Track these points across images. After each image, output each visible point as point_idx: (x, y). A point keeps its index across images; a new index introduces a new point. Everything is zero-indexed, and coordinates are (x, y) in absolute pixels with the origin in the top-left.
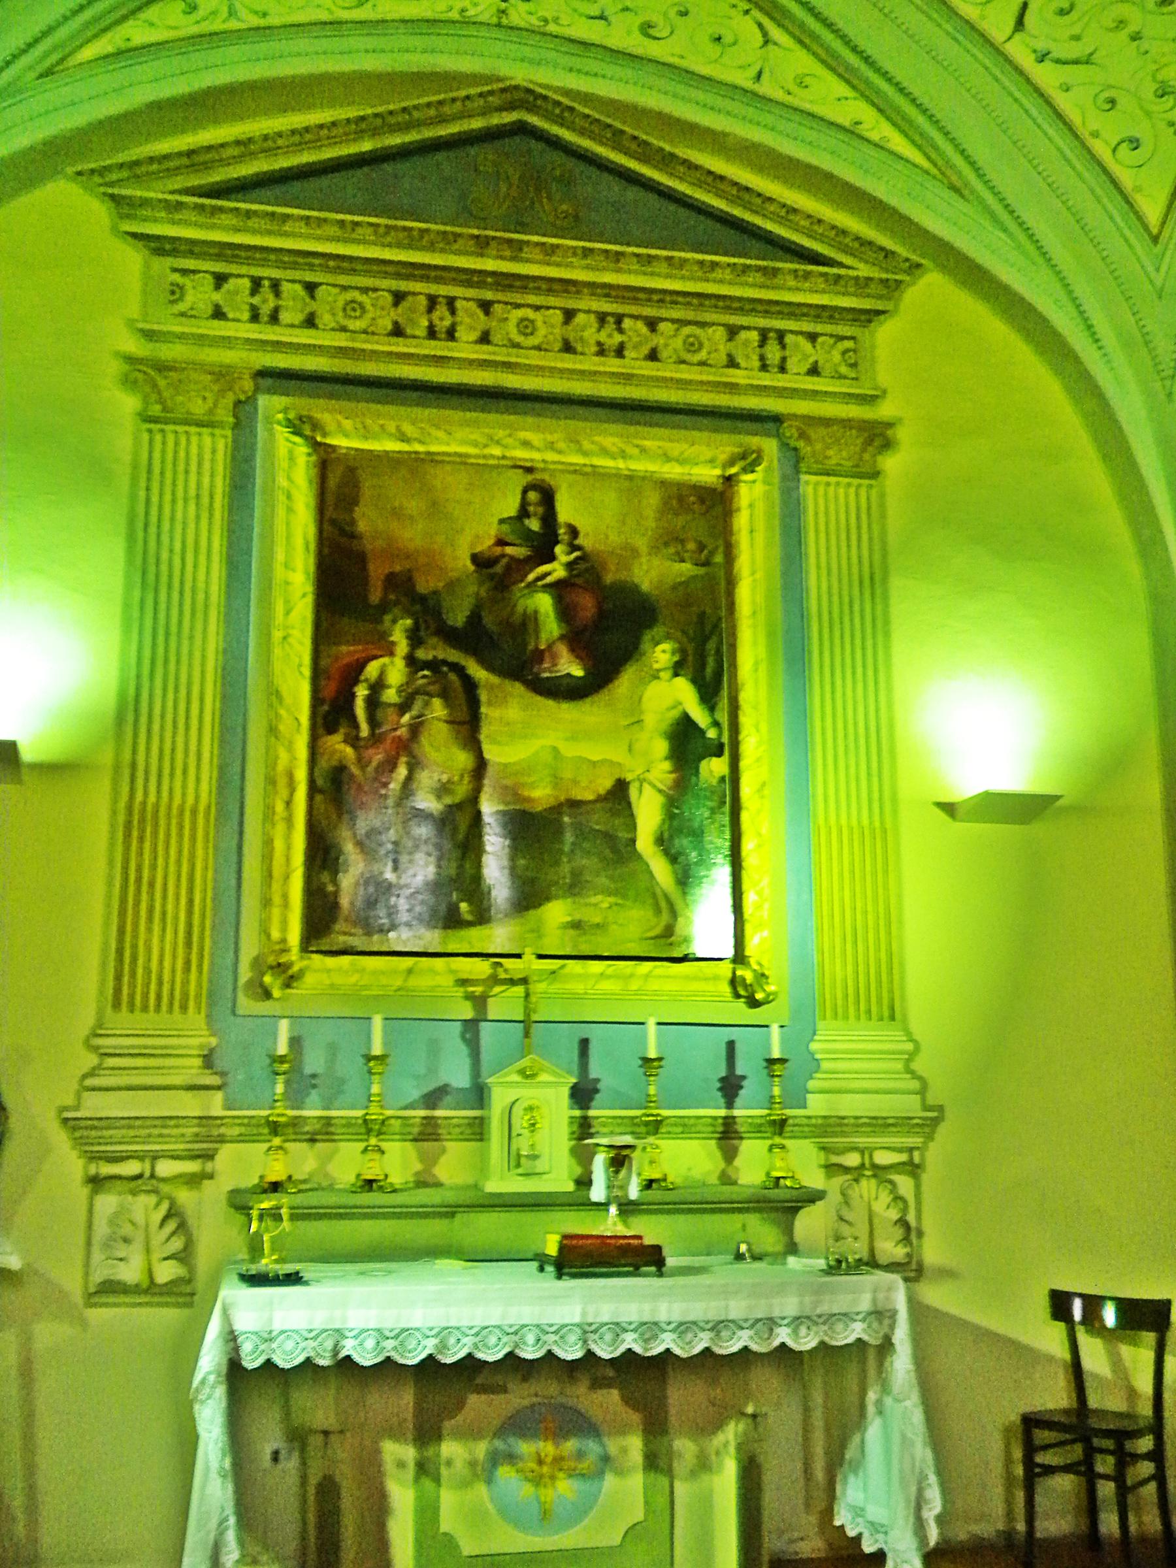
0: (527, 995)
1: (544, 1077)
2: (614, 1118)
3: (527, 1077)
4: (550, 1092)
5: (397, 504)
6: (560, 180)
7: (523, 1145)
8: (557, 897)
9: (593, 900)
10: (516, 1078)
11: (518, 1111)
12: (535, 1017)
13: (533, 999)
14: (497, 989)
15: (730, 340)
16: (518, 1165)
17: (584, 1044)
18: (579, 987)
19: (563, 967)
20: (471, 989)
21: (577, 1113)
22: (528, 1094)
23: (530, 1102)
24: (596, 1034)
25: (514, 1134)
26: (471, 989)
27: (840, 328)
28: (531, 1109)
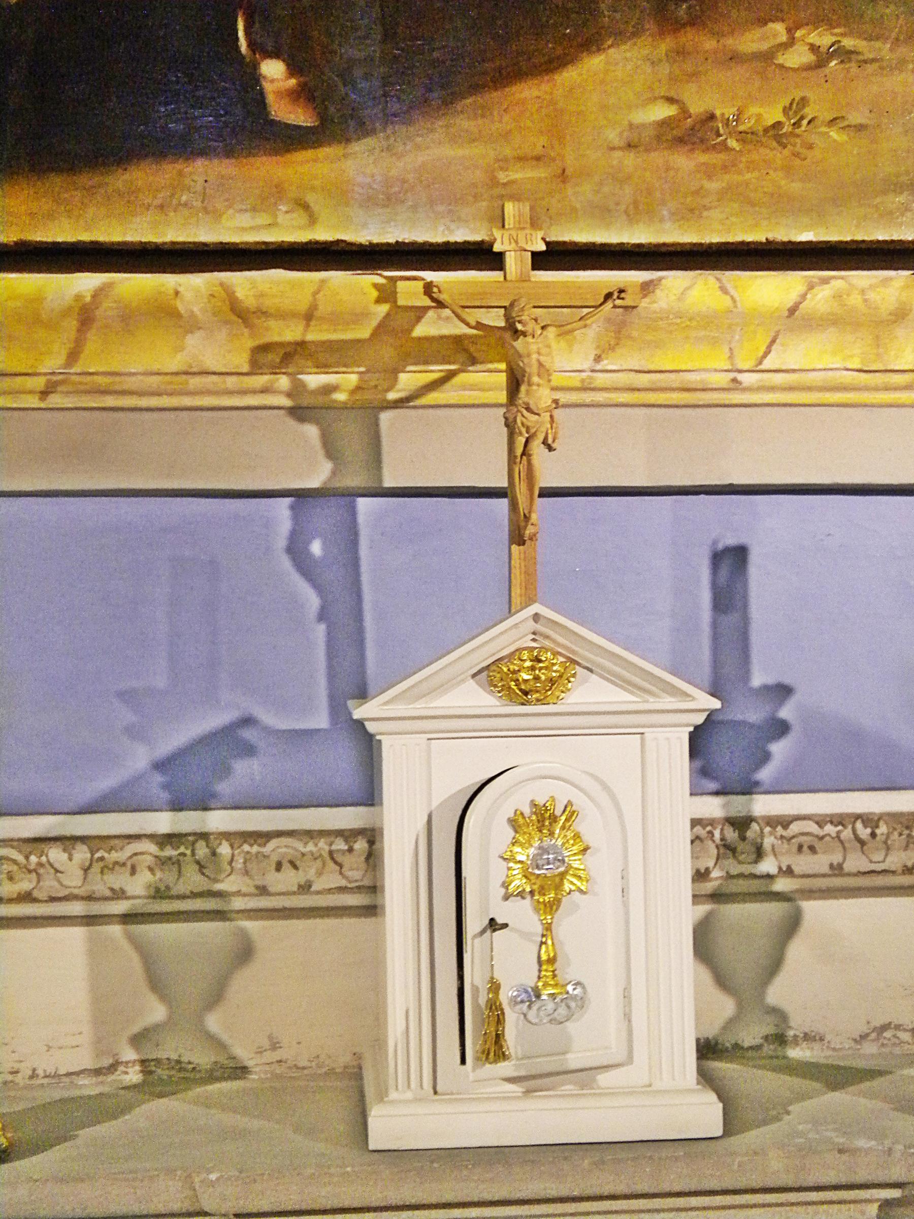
0: (515, 382)
1: (587, 693)
2: (839, 820)
3: (525, 694)
4: (613, 755)
5: (370, 226)
6: (507, 888)
7: (508, 963)
8: (621, 36)
9: (751, 41)
10: (478, 698)
11: (487, 832)
12: (550, 471)
13: (540, 395)
14: (410, 379)
15: (532, 801)
16: (495, 1049)
17: (732, 560)
18: (706, 364)
19: (647, 288)
20: (314, 380)
21: (713, 807)
22: (538, 762)
23: (541, 793)
24: (769, 530)
25: (473, 924)
26: (314, 380)
27: (698, 378)
28: (544, 818)
